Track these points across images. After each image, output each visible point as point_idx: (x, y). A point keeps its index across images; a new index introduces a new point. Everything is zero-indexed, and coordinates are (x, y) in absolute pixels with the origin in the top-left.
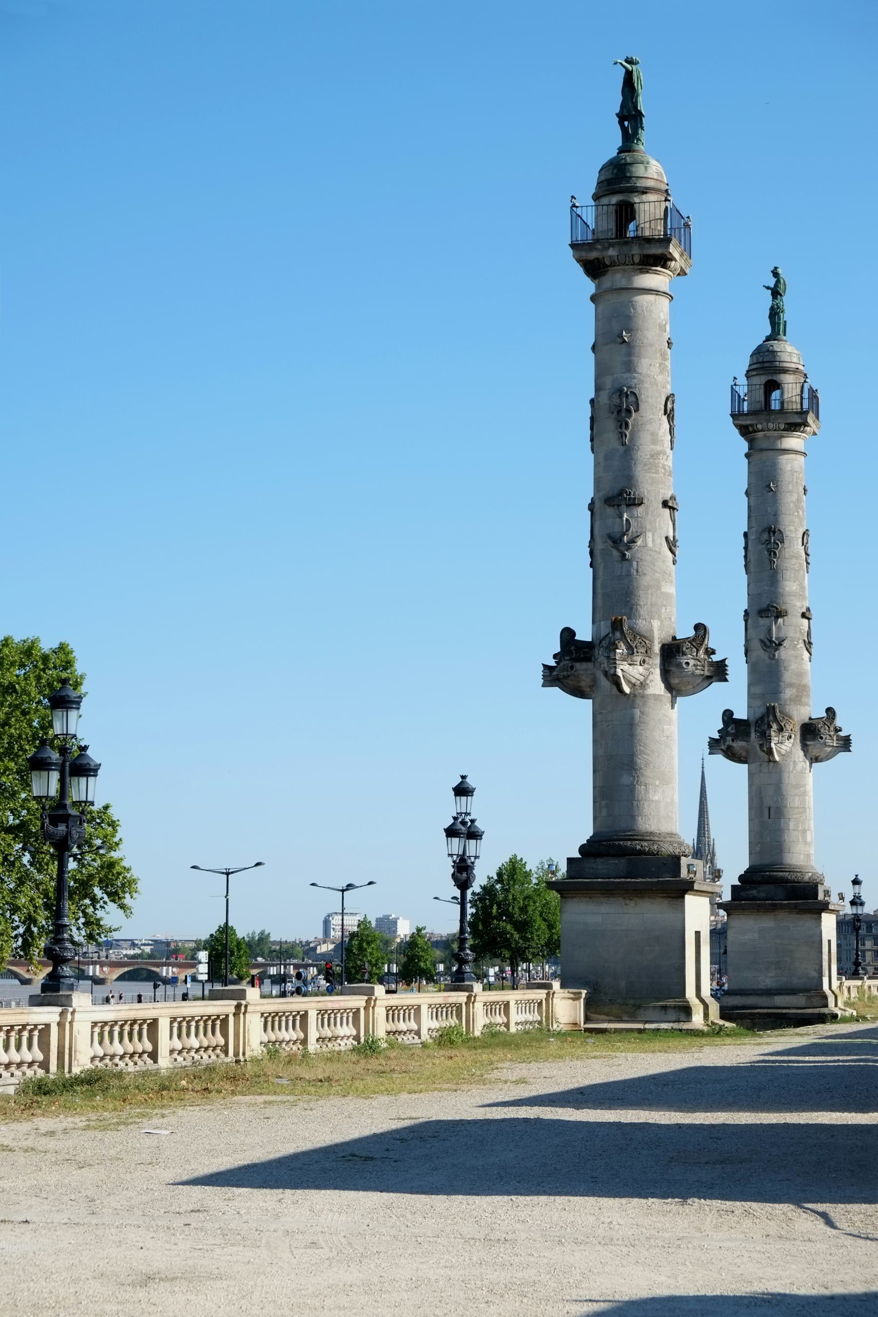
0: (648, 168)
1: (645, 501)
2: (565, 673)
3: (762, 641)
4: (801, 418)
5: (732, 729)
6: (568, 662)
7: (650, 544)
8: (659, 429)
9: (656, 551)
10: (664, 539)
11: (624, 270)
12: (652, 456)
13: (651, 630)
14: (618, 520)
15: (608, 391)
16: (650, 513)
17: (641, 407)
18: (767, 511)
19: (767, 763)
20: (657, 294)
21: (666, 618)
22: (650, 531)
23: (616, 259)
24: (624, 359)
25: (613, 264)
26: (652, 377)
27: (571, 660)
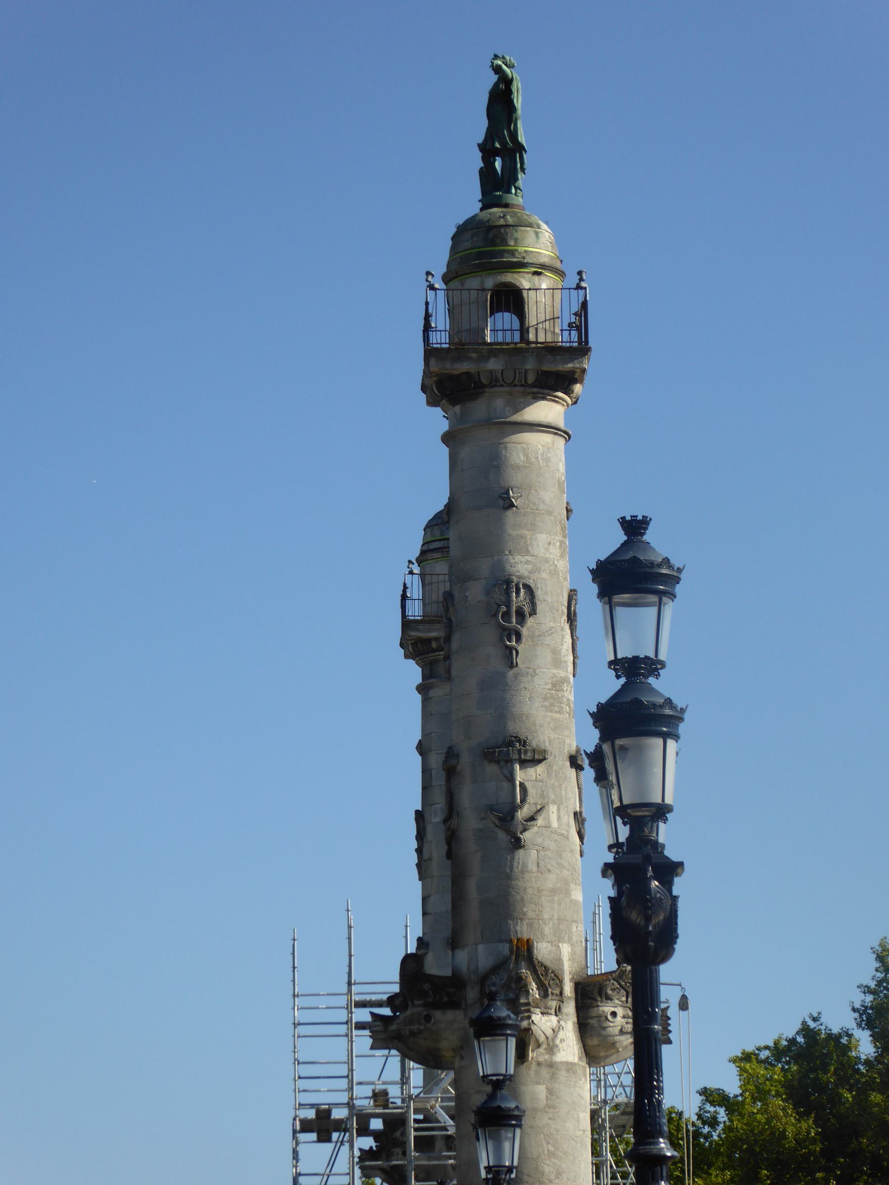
0: (540, 235)
1: (550, 759)
2: (415, 1028)
6: (420, 1009)
7: (555, 824)
8: (562, 645)
9: (562, 835)
10: (572, 816)
12: (554, 685)
13: (559, 960)
14: (505, 785)
16: (553, 775)
17: (540, 607)
20: (556, 434)
21: (577, 942)
22: (554, 802)
26: (551, 562)
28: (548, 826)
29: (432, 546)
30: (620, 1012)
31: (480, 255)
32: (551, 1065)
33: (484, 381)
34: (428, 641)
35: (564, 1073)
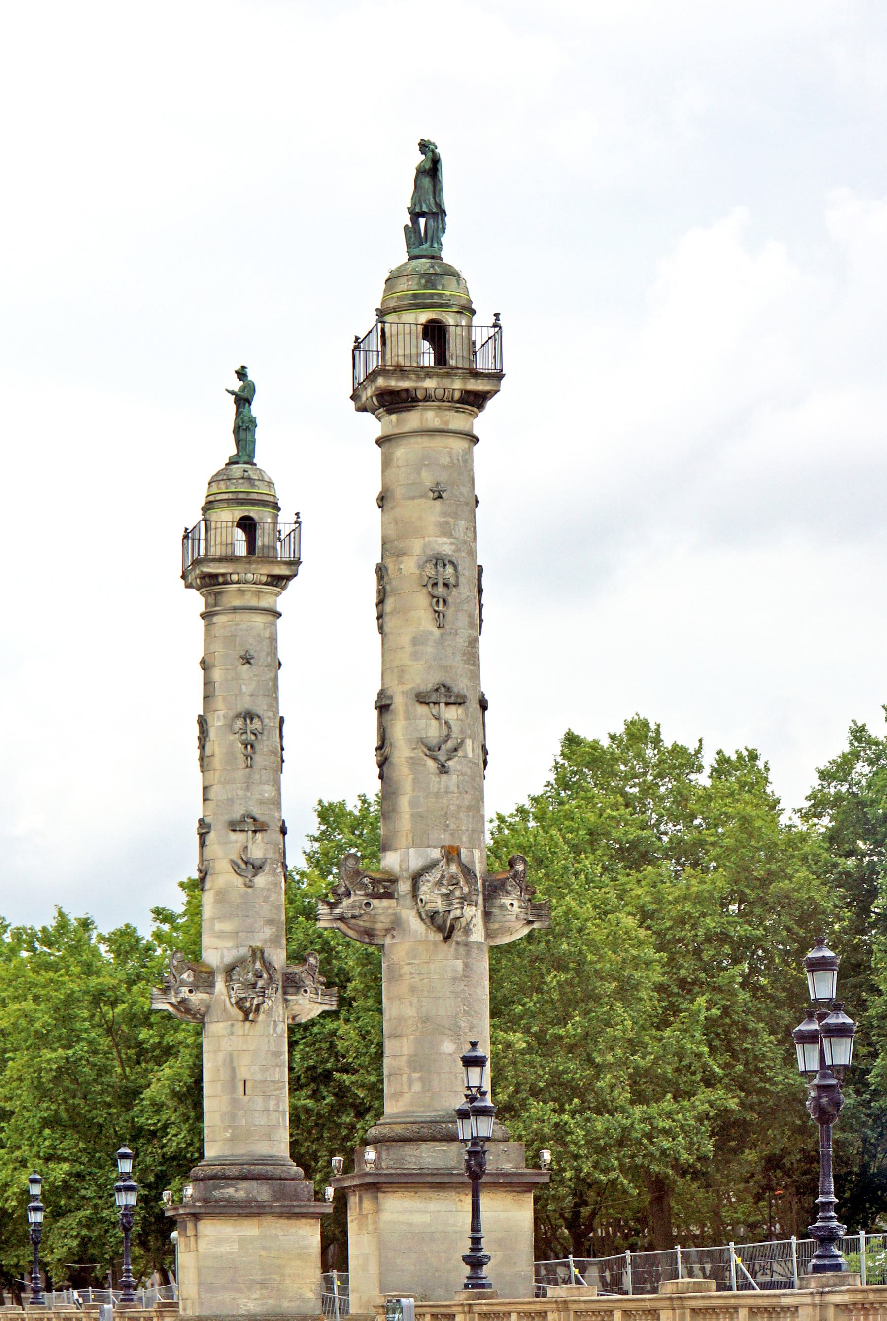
2: (357, 912)
3: (233, 862)
4: (291, 570)
5: (188, 976)
6: (362, 898)
7: (470, 755)
9: (475, 763)
11: (439, 408)
15: (417, 557)
18: (241, 690)
19: (241, 1024)
22: (470, 737)
23: (433, 394)
24: (439, 519)
25: (427, 398)
27: (366, 895)
28: (465, 757)
30: (516, 903)
31: (415, 296)
32: (467, 944)
33: (419, 397)
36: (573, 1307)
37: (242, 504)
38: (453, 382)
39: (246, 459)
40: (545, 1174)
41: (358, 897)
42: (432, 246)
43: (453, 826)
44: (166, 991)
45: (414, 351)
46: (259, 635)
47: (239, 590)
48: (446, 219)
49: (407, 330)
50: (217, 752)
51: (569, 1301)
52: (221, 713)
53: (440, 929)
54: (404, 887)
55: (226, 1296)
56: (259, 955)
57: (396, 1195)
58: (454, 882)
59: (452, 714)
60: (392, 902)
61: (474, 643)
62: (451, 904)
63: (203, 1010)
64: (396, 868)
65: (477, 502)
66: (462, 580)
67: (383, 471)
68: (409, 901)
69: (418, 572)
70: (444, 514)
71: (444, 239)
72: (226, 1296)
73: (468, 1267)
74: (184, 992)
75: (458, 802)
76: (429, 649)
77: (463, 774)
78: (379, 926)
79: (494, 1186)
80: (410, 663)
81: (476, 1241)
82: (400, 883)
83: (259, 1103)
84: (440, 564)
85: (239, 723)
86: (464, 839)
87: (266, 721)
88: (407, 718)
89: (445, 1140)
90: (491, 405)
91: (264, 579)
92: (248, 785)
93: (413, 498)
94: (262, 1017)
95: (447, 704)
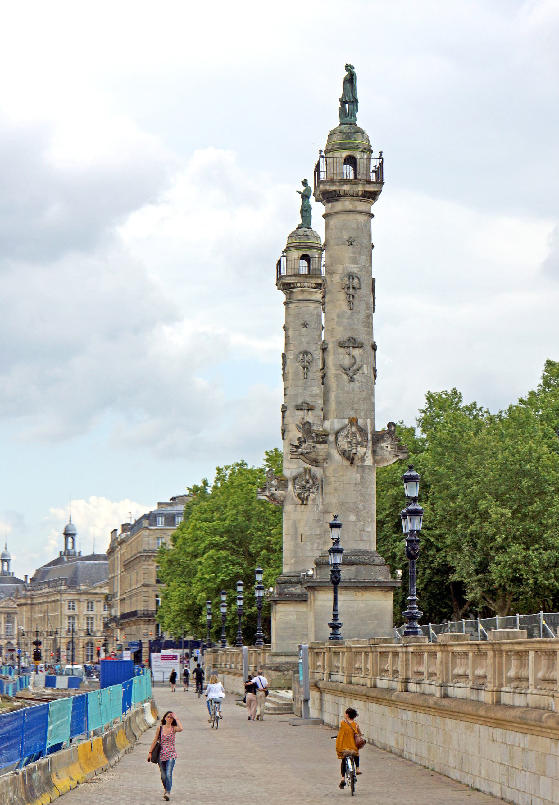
2: (309, 451)
3: (297, 425)
7: (366, 373)
11: (352, 200)
18: (302, 340)
22: (366, 364)
25: (345, 195)
27: (313, 442)
29: (292, 245)
30: (389, 446)
31: (340, 143)
32: (363, 467)
34: (290, 284)
35: (367, 470)
36: (354, 650)
37: (303, 248)
38: (358, 187)
39: (306, 226)
40: (399, 582)
41: (309, 443)
42: (351, 118)
43: (356, 408)
44: (264, 489)
45: (338, 171)
46: (311, 314)
47: (301, 291)
48: (359, 104)
49: (335, 161)
50: (290, 371)
51: (353, 647)
52: (292, 352)
53: (348, 459)
54: (332, 438)
55: (289, 642)
56: (308, 471)
57: (323, 592)
58: (353, 435)
59: (356, 352)
60: (326, 446)
61: (369, 317)
62: (351, 447)
63: (282, 499)
64: (329, 429)
65: (373, 247)
66: (362, 285)
67: (326, 231)
68: (334, 445)
69: (340, 282)
70: (354, 253)
71: (357, 115)
72: (289, 642)
73: (331, 629)
74: (273, 490)
75: (359, 396)
76: (345, 320)
77: (362, 382)
78: (320, 457)
79: (346, 588)
80: (336, 327)
81: (335, 616)
82: (330, 436)
83: (309, 546)
84: (351, 278)
85: (301, 357)
86: (362, 414)
87: (315, 356)
88: (334, 354)
89: (350, 565)
90: (380, 197)
91: (313, 285)
92: (305, 387)
93: (338, 245)
94: (310, 502)
95: (354, 347)
